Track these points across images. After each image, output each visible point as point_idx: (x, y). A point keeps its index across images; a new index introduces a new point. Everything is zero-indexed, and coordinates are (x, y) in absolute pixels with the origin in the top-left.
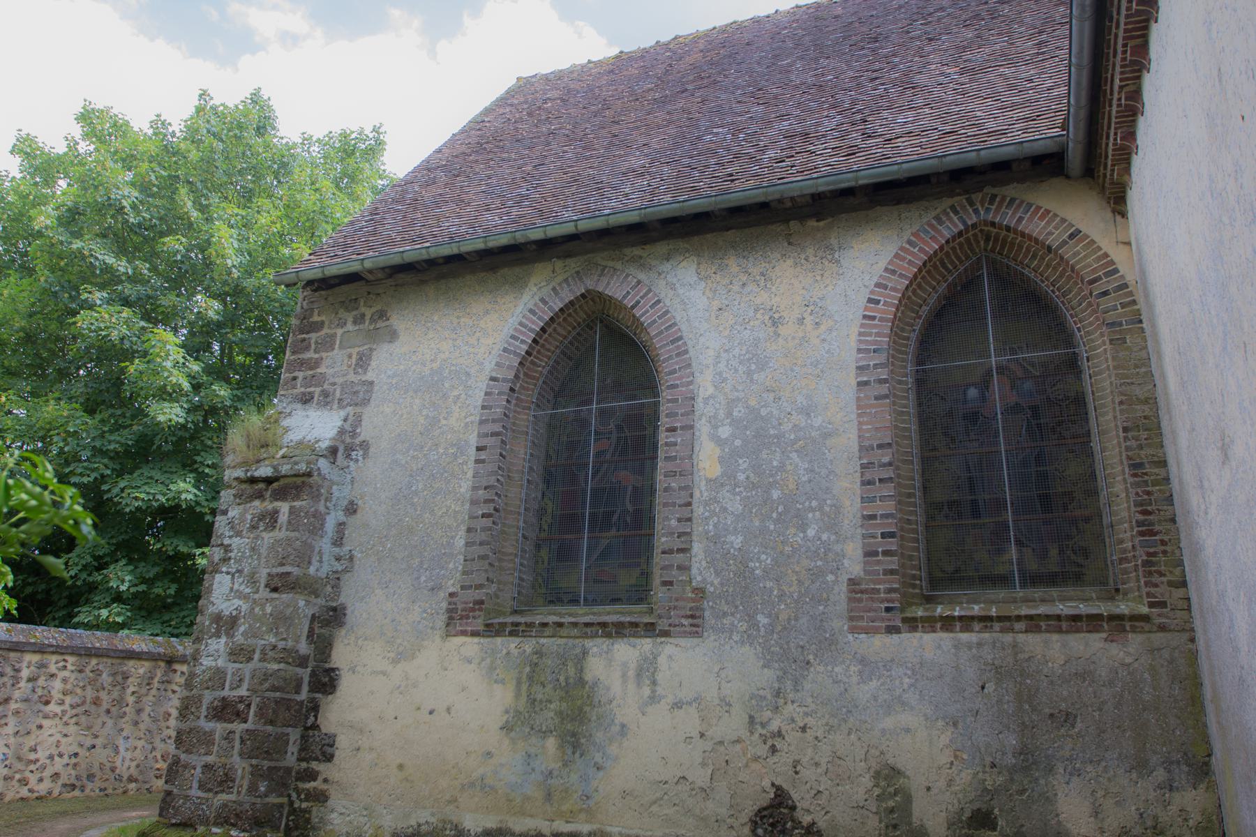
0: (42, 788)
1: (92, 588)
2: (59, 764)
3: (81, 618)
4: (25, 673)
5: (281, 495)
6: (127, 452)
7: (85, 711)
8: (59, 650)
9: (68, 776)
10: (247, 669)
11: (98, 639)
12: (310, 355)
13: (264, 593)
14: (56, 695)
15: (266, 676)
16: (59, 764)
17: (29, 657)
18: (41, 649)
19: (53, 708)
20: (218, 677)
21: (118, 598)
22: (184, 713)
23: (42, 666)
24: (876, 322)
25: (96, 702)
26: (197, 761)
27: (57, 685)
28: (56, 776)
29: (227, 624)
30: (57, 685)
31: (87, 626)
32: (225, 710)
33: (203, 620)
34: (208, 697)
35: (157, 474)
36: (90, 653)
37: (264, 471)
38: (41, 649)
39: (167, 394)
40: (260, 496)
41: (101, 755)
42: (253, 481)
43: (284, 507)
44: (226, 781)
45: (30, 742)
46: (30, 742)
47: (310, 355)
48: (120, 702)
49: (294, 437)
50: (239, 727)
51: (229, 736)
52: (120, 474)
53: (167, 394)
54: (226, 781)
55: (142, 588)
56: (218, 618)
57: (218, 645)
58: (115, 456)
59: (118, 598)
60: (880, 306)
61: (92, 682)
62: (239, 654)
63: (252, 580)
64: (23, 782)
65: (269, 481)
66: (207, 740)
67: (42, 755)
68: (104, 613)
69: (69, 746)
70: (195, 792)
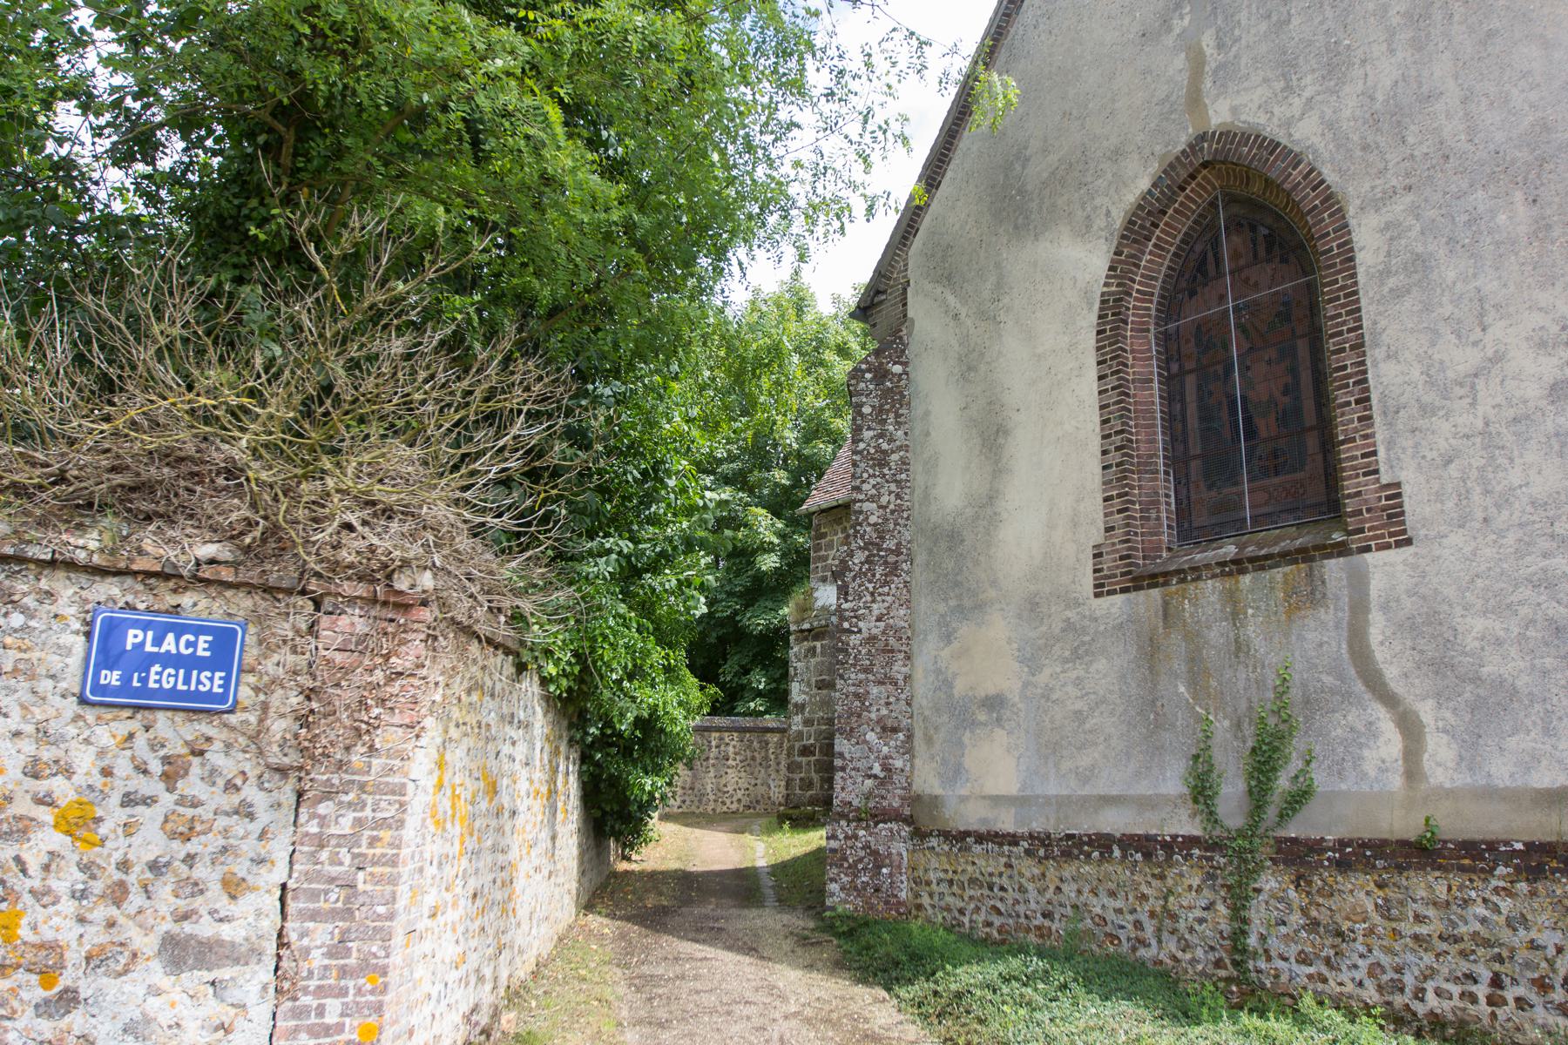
0: (734, 807)
1: (743, 687)
2: (740, 794)
3: (740, 709)
4: (714, 743)
5: (817, 637)
6: (748, 590)
7: (748, 764)
8: (728, 729)
9: (746, 800)
10: (812, 729)
11: (748, 722)
12: (823, 553)
13: (815, 691)
14: (732, 756)
15: (821, 732)
16: (740, 794)
17: (715, 735)
18: (719, 729)
19: (730, 762)
20: (800, 734)
21: (759, 694)
22: (789, 755)
23: (721, 739)
24: (1358, 453)
25: (753, 759)
26: (797, 776)
27: (731, 749)
28: (739, 801)
29: (800, 708)
30: (731, 749)
31: (744, 715)
32: (806, 751)
33: (790, 707)
34: (797, 745)
35: (769, 604)
36: (742, 730)
37: (806, 626)
38: (719, 729)
39: (767, 548)
40: (806, 639)
41: (762, 790)
42: (802, 631)
43: (818, 644)
44: (810, 785)
45: (723, 781)
46: (723, 781)
47: (823, 553)
48: (766, 758)
49: (819, 604)
50: (812, 759)
51: (809, 763)
52: (747, 606)
53: (767, 548)
54: (810, 785)
55: (773, 685)
56: (796, 705)
57: (798, 719)
58: (741, 595)
59: (759, 694)
60: (1359, 442)
61: (749, 747)
62: (808, 722)
63: (809, 685)
64: (724, 803)
65: (809, 631)
66: (799, 766)
67: (730, 788)
68: (752, 705)
69: (743, 784)
70: (798, 791)
